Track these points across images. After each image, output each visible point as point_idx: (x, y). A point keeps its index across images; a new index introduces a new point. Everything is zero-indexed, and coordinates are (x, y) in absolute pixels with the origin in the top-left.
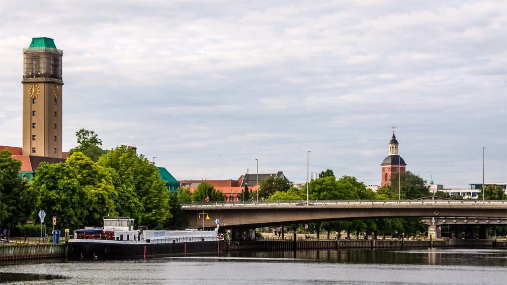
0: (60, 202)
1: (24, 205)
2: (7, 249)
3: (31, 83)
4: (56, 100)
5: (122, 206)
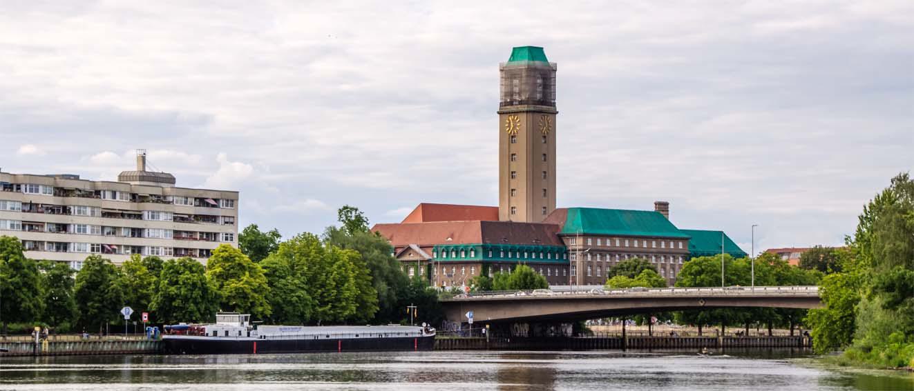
0: (180, 298)
1: (109, 302)
2: (62, 345)
3: (509, 113)
4: (545, 137)
5: (284, 300)
